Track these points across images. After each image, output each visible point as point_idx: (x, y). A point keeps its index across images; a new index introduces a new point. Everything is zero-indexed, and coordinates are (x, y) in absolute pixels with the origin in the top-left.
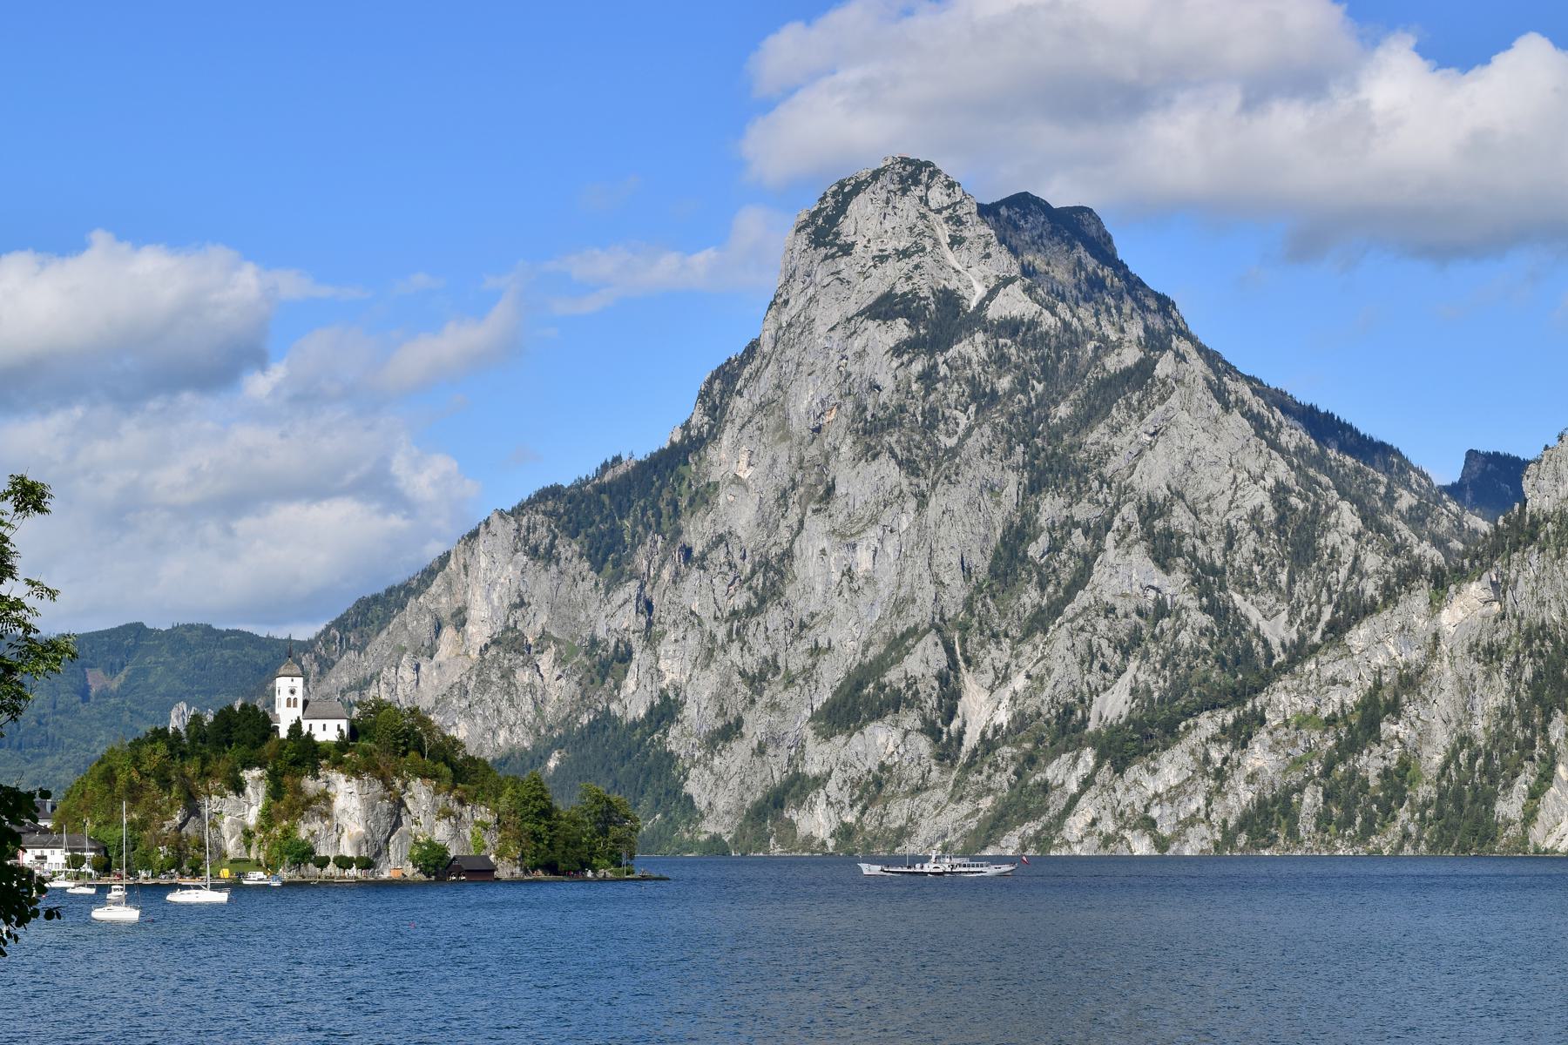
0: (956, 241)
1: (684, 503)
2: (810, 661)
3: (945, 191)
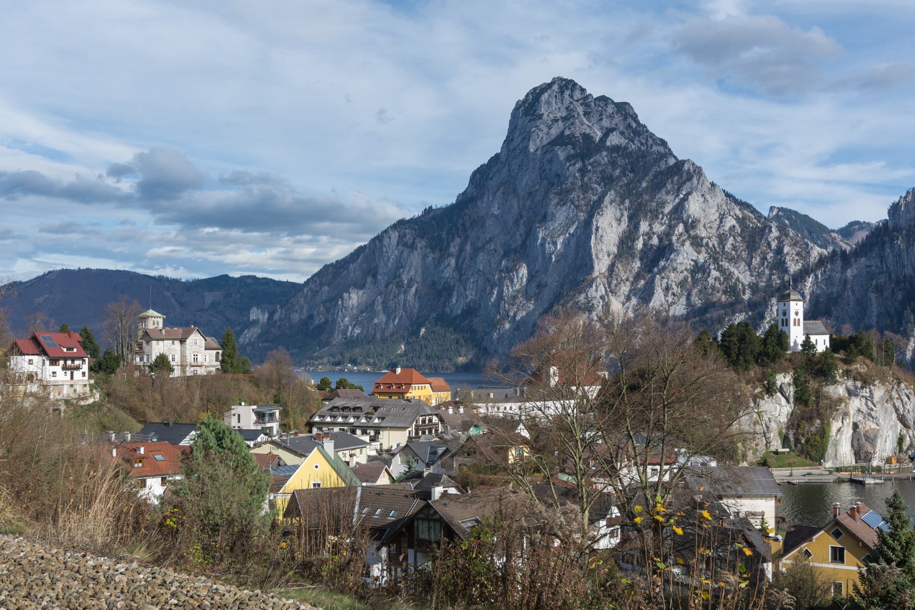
0: (586, 114)
1: (468, 225)
3: (579, 92)
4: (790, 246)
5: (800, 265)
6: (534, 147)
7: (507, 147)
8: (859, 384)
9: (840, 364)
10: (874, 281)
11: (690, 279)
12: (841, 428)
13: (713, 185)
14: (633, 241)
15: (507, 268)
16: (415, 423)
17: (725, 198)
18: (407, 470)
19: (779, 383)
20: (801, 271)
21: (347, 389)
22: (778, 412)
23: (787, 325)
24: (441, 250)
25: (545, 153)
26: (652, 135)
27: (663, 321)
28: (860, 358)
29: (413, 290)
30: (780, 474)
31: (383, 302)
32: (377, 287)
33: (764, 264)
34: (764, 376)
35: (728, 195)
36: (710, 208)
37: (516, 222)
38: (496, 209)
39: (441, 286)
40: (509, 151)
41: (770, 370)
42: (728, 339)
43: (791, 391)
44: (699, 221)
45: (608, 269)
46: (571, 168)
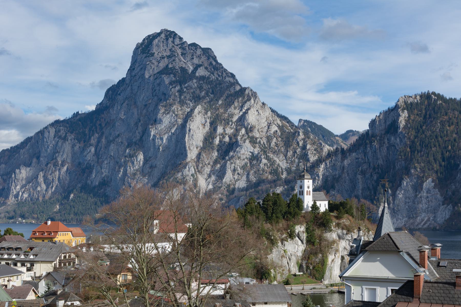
0: (183, 54)
1: (103, 125)
2: (150, 170)
3: (179, 40)
4: (311, 144)
5: (317, 157)
6: (148, 74)
7: (130, 73)
8: (345, 232)
9: (334, 219)
10: (360, 168)
11: (249, 165)
12: (334, 259)
13: (263, 104)
14: (213, 139)
15: (130, 155)
16: (58, 258)
17: (271, 113)
18: (47, 290)
19: (297, 231)
20: (317, 160)
21: (12, 235)
22: (296, 250)
23: (302, 195)
24: (84, 142)
25: (156, 79)
26: (225, 70)
27: (231, 191)
28: (346, 215)
29: (65, 168)
30: (296, 288)
31: (44, 176)
32: (40, 166)
33: (294, 156)
34: (288, 227)
35: (273, 111)
36: (262, 119)
37: (136, 124)
38: (123, 115)
39: (85, 166)
40: (131, 76)
41: (291, 223)
42: (267, 203)
43: (304, 236)
44: (255, 127)
45: (197, 157)
46: (173, 90)
